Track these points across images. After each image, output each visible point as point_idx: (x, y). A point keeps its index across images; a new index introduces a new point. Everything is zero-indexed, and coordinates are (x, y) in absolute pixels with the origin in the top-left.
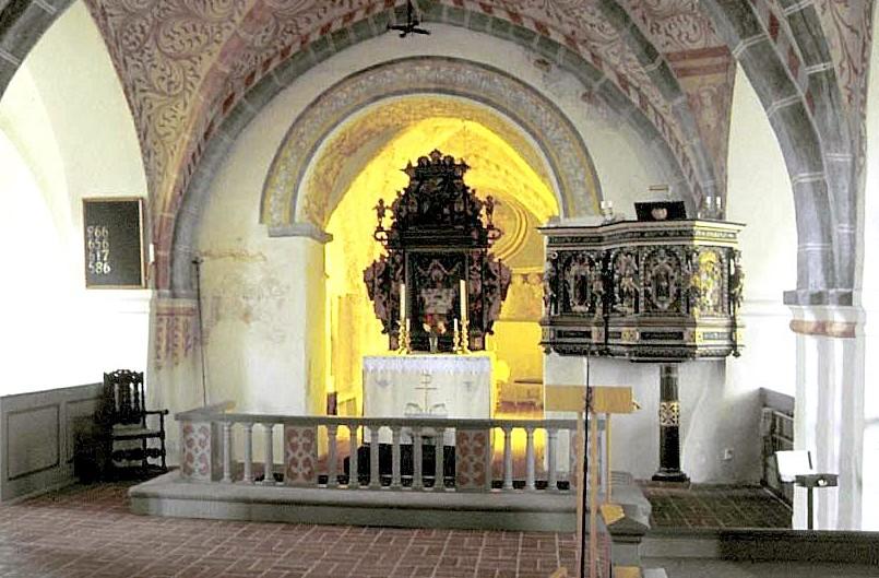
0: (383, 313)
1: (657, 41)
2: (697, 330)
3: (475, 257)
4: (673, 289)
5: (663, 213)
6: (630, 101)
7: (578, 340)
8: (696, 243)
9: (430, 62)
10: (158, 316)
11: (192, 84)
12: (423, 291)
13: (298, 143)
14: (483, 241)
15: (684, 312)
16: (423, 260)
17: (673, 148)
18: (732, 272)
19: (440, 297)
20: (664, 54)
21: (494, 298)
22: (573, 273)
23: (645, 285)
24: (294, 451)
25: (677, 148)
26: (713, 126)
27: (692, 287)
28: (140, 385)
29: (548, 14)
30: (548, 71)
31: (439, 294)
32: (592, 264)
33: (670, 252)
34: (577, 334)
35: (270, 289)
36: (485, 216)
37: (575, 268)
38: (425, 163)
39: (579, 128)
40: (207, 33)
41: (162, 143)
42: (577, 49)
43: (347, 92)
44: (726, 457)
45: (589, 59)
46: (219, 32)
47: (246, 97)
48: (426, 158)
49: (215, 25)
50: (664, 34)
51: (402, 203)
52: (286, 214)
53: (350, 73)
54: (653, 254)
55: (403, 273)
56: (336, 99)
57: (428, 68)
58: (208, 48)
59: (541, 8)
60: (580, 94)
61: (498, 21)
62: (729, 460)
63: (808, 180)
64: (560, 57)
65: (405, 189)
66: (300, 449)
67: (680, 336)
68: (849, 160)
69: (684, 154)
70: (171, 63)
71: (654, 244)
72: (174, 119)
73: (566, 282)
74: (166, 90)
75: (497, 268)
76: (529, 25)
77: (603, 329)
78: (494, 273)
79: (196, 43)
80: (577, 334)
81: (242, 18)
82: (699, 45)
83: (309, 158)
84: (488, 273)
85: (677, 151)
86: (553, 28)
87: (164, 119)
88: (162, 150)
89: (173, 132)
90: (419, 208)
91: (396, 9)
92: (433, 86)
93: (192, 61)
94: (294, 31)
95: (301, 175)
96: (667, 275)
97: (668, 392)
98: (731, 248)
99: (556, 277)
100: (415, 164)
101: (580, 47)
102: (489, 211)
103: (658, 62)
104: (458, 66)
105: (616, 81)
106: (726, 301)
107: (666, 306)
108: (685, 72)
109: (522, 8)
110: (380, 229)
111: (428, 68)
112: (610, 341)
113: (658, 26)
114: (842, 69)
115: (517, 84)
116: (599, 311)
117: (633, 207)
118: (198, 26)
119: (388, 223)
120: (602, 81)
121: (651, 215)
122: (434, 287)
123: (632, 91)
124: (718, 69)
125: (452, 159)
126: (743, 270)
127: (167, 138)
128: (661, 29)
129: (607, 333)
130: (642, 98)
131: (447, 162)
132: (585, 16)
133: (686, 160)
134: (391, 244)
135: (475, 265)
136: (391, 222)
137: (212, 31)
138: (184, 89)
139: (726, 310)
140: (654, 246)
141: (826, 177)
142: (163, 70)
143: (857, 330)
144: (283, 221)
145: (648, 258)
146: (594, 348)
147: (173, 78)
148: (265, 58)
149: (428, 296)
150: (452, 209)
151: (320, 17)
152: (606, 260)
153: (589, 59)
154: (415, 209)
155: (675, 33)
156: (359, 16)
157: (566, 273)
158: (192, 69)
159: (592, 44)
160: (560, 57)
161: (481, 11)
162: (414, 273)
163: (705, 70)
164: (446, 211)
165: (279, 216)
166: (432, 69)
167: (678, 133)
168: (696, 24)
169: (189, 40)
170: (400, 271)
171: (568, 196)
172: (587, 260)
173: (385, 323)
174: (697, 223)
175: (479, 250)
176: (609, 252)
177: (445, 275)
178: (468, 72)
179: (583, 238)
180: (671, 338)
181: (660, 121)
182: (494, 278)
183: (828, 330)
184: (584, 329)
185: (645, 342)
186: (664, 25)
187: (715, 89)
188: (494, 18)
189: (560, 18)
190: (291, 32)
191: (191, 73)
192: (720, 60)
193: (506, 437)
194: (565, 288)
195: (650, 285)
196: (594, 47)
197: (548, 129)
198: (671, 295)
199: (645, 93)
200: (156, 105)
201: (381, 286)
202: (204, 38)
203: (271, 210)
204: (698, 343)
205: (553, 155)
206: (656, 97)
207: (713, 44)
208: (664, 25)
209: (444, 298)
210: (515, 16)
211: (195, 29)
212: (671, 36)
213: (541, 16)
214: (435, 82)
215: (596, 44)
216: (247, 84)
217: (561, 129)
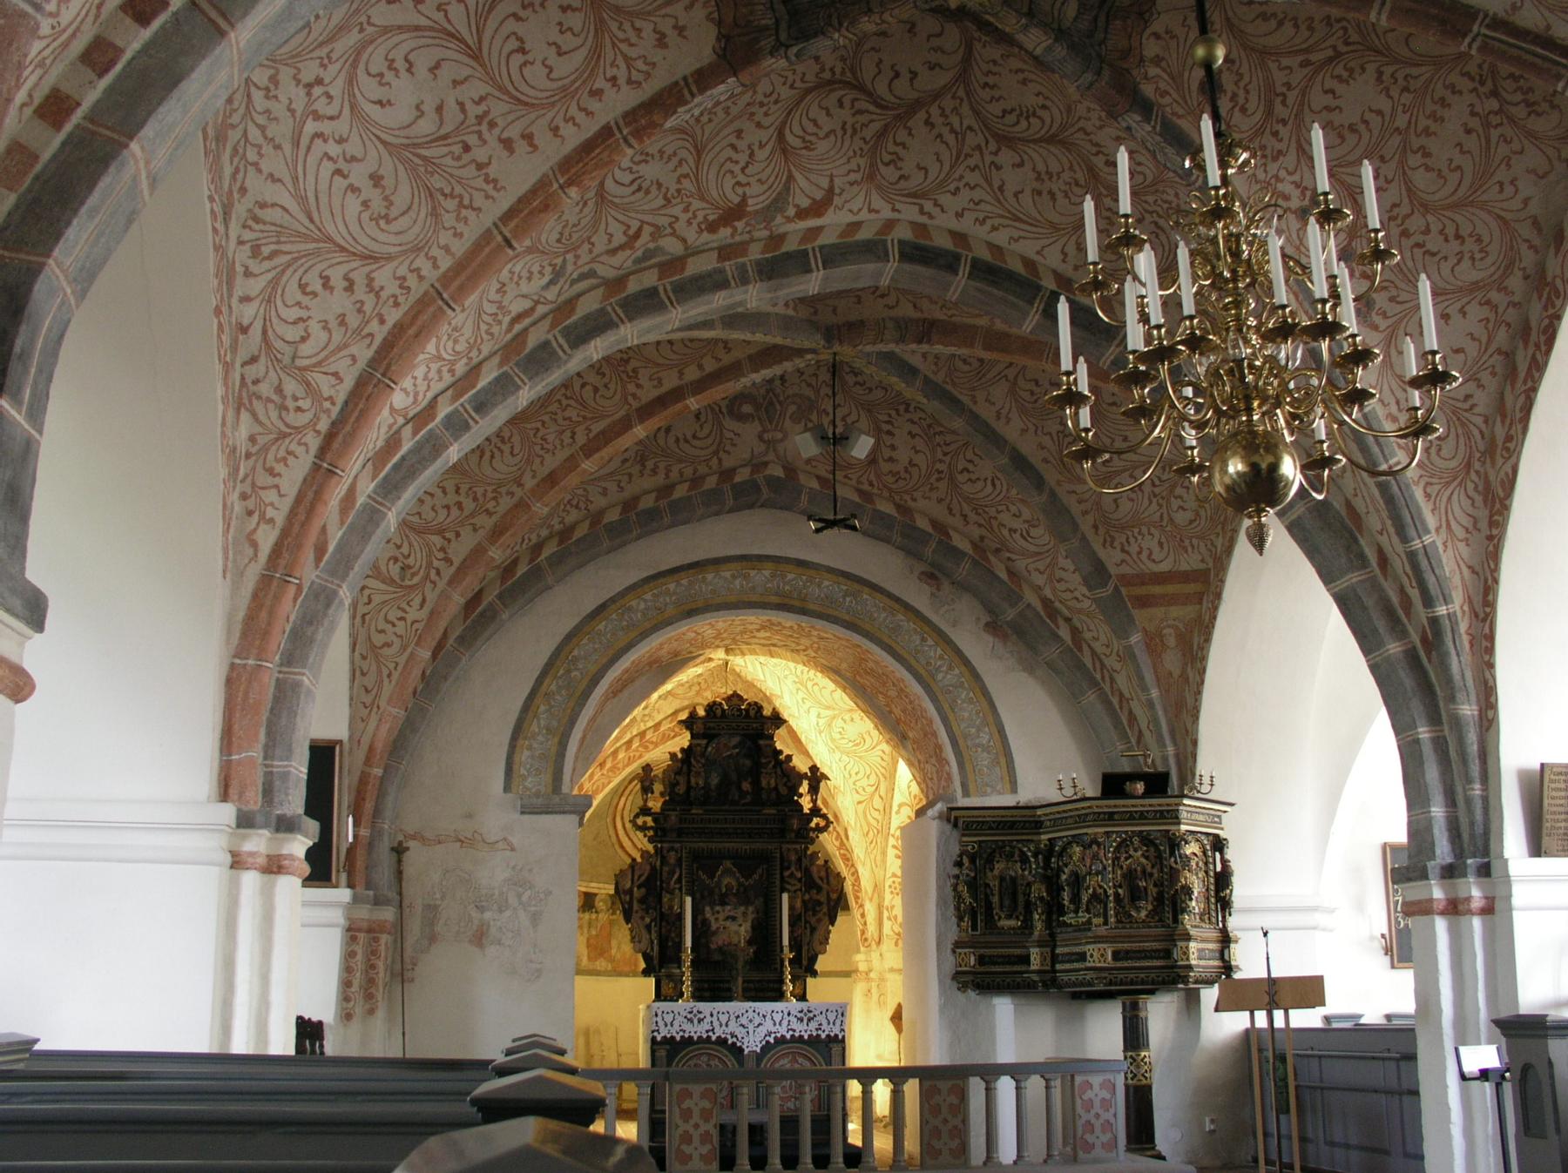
0: (644, 945)
1: (1111, 558)
2: (1192, 945)
3: (793, 858)
4: (1153, 891)
5: (1140, 787)
6: (1058, 637)
7: (1008, 968)
8: (1184, 828)
9: (770, 565)
10: (352, 932)
11: (438, 573)
12: (707, 909)
13: (569, 671)
15: (1170, 922)
16: (705, 862)
17: (1115, 701)
18: (1219, 868)
19: (734, 919)
20: (1117, 576)
21: (819, 921)
22: (996, 872)
23: (1115, 886)
24: (686, 1121)
25: (1121, 701)
26: (1176, 672)
27: (1183, 887)
29: (950, 510)
30: (938, 590)
31: (731, 914)
32: (1024, 860)
33: (1146, 840)
34: (1009, 960)
35: (519, 896)
36: (808, 798)
37: (999, 867)
38: (719, 712)
39: (980, 669)
40: (475, 499)
41: (376, 656)
42: (987, 560)
43: (645, 601)
44: (1208, 1126)
45: (1003, 575)
46: (495, 498)
47: (500, 596)
49: (490, 489)
50: (1119, 548)
51: (678, 773)
52: (547, 778)
53: (652, 572)
55: (679, 880)
56: (630, 609)
57: (728, 574)
58: (472, 521)
59: (940, 501)
60: (983, 622)
61: (882, 516)
62: (1212, 1132)
63: (1427, 735)
64: (963, 570)
65: (683, 750)
66: (696, 1118)
67: (1167, 954)
68: (1476, 713)
69: (1131, 712)
70: (412, 535)
71: (1125, 829)
72: (402, 623)
73: (987, 885)
74: (397, 578)
75: (823, 874)
76: (922, 523)
77: (1048, 950)
78: (819, 882)
79: (455, 512)
81: (535, 481)
82: (1164, 567)
83: (586, 695)
84: (810, 884)
85: (1121, 708)
86: (955, 529)
87: (387, 621)
88: (374, 667)
89: (397, 643)
90: (707, 778)
91: (734, 487)
92: (774, 599)
93: (444, 538)
94: (582, 505)
95: (572, 722)
96: (1144, 871)
97: (1134, 1037)
98: (1216, 836)
99: (975, 878)
100: (701, 712)
101: (992, 558)
102: (814, 790)
103: (1110, 588)
104: (812, 572)
105: (1039, 608)
106: (1213, 907)
107: (1143, 914)
108: (1144, 602)
109: (914, 500)
110: (645, 811)
111: (766, 573)
112: (1058, 967)
113: (1113, 539)
114: (1464, 612)
115: (892, 603)
116: (1039, 926)
118: (464, 488)
119: (656, 804)
120: (1021, 606)
121: (1124, 789)
122: (723, 903)
123: (1061, 622)
124: (1185, 600)
126: (1234, 865)
127: (386, 651)
128: (1116, 544)
129: (1055, 959)
130: (1075, 632)
131: (752, 713)
132: (1005, 518)
133: (1132, 718)
134: (660, 832)
135: (793, 869)
137: (484, 495)
138: (427, 576)
139: (1214, 920)
140: (1126, 832)
141: (1447, 732)
142: (399, 547)
143: (1498, 905)
144: (543, 790)
145: (1118, 849)
146: (1035, 977)
147: (411, 561)
148: (534, 540)
149: (716, 917)
150: (756, 783)
151: (621, 489)
152: (1049, 851)
153: (1003, 575)
154: (701, 783)
155: (1134, 549)
156: (680, 492)
157: (989, 874)
158: (442, 549)
159: (1008, 555)
160: (963, 570)
161: (857, 499)
163: (1172, 600)
164: (746, 786)
165: (534, 782)
166: (773, 576)
167: (1121, 681)
168: (1163, 540)
169: (447, 507)
170: (676, 876)
171: (968, 767)
172: (1017, 852)
173: (647, 958)
174: (1186, 801)
175: (798, 847)
177: (740, 884)
178: (826, 583)
179: (1014, 823)
181: (1098, 665)
182: (819, 889)
183: (1461, 907)
184: (1018, 951)
185: (1119, 964)
186: (1120, 538)
187: (1181, 626)
188: (875, 510)
189: (965, 517)
190: (577, 507)
191: (441, 555)
192: (1191, 588)
193: (987, 1089)
194: (986, 895)
195: (1120, 886)
196: (1009, 559)
197: (938, 669)
198: (1150, 898)
199: (1078, 625)
200: (377, 599)
201: (642, 901)
202: (469, 505)
203: (523, 771)
204: (1193, 962)
205: (946, 706)
206: (1099, 633)
207: (1184, 567)
208: (1120, 538)
210: (903, 509)
211: (457, 492)
212: (1128, 553)
213: (939, 512)
214: (777, 594)
215: (1014, 557)
216: (504, 579)
217: (957, 671)
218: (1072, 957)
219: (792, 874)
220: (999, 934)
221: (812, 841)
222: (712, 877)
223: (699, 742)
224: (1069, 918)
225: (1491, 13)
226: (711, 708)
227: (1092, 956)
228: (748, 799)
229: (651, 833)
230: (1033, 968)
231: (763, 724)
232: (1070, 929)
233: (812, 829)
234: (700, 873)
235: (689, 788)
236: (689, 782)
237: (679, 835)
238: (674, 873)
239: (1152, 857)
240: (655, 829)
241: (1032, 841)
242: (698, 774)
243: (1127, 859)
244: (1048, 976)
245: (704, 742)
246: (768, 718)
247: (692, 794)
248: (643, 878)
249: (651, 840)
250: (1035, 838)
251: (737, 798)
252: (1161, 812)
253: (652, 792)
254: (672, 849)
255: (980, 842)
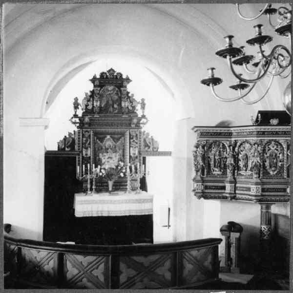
7: (217, 191)
12: (100, 154)
14: (138, 126)
19: (111, 158)
28: (89, 165)
31: (110, 156)
34: (217, 188)
38: (105, 76)
48: (106, 73)
54: (269, 142)
65: (91, 92)
73: (209, 157)
75: (151, 141)
77: (234, 185)
78: (149, 144)
80: (217, 188)
99: (204, 155)
110: (76, 116)
117: (148, 191)
119: (80, 113)
125: (121, 75)
129: (235, 188)
131: (118, 77)
134: (82, 124)
135: (134, 139)
136: (82, 112)
146: (228, 195)
150: (120, 105)
162: (95, 143)
170: (88, 142)
172: (221, 145)
176: (236, 142)
180: (280, 192)
209: (114, 158)
218: (243, 189)
219: (134, 141)
220: (213, 177)
221: (141, 128)
222: (102, 142)
223: (96, 88)
224: (242, 172)
225: (89, 192)
226: (102, 74)
227: (253, 190)
228: (116, 111)
229: (78, 125)
230: (226, 191)
231: (123, 81)
232: (243, 177)
233: (142, 123)
234: (98, 140)
235: (93, 107)
236: (93, 104)
237: (90, 126)
238: (88, 140)
239: (279, 150)
240: (80, 124)
241: (228, 140)
242: (97, 101)
243: (269, 150)
244: (232, 195)
245: (99, 89)
246: (125, 79)
247: (94, 109)
248: (69, 144)
249: (78, 127)
250: (229, 139)
251: (112, 111)
252: (285, 132)
253: (78, 108)
254: (87, 131)
255: (207, 140)
